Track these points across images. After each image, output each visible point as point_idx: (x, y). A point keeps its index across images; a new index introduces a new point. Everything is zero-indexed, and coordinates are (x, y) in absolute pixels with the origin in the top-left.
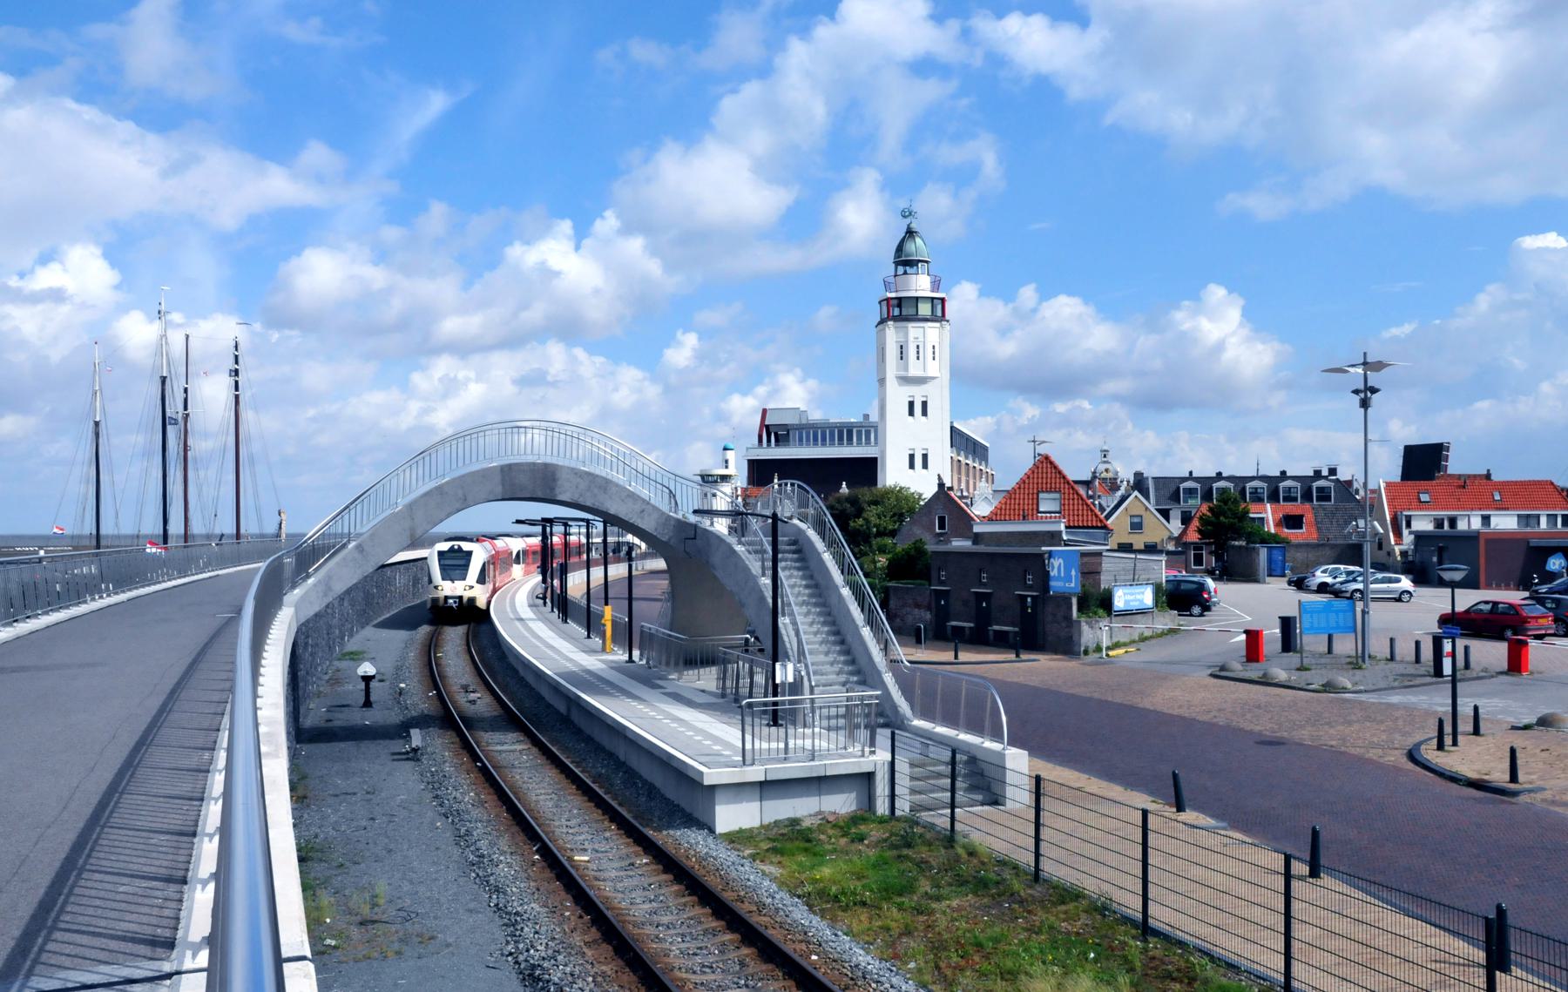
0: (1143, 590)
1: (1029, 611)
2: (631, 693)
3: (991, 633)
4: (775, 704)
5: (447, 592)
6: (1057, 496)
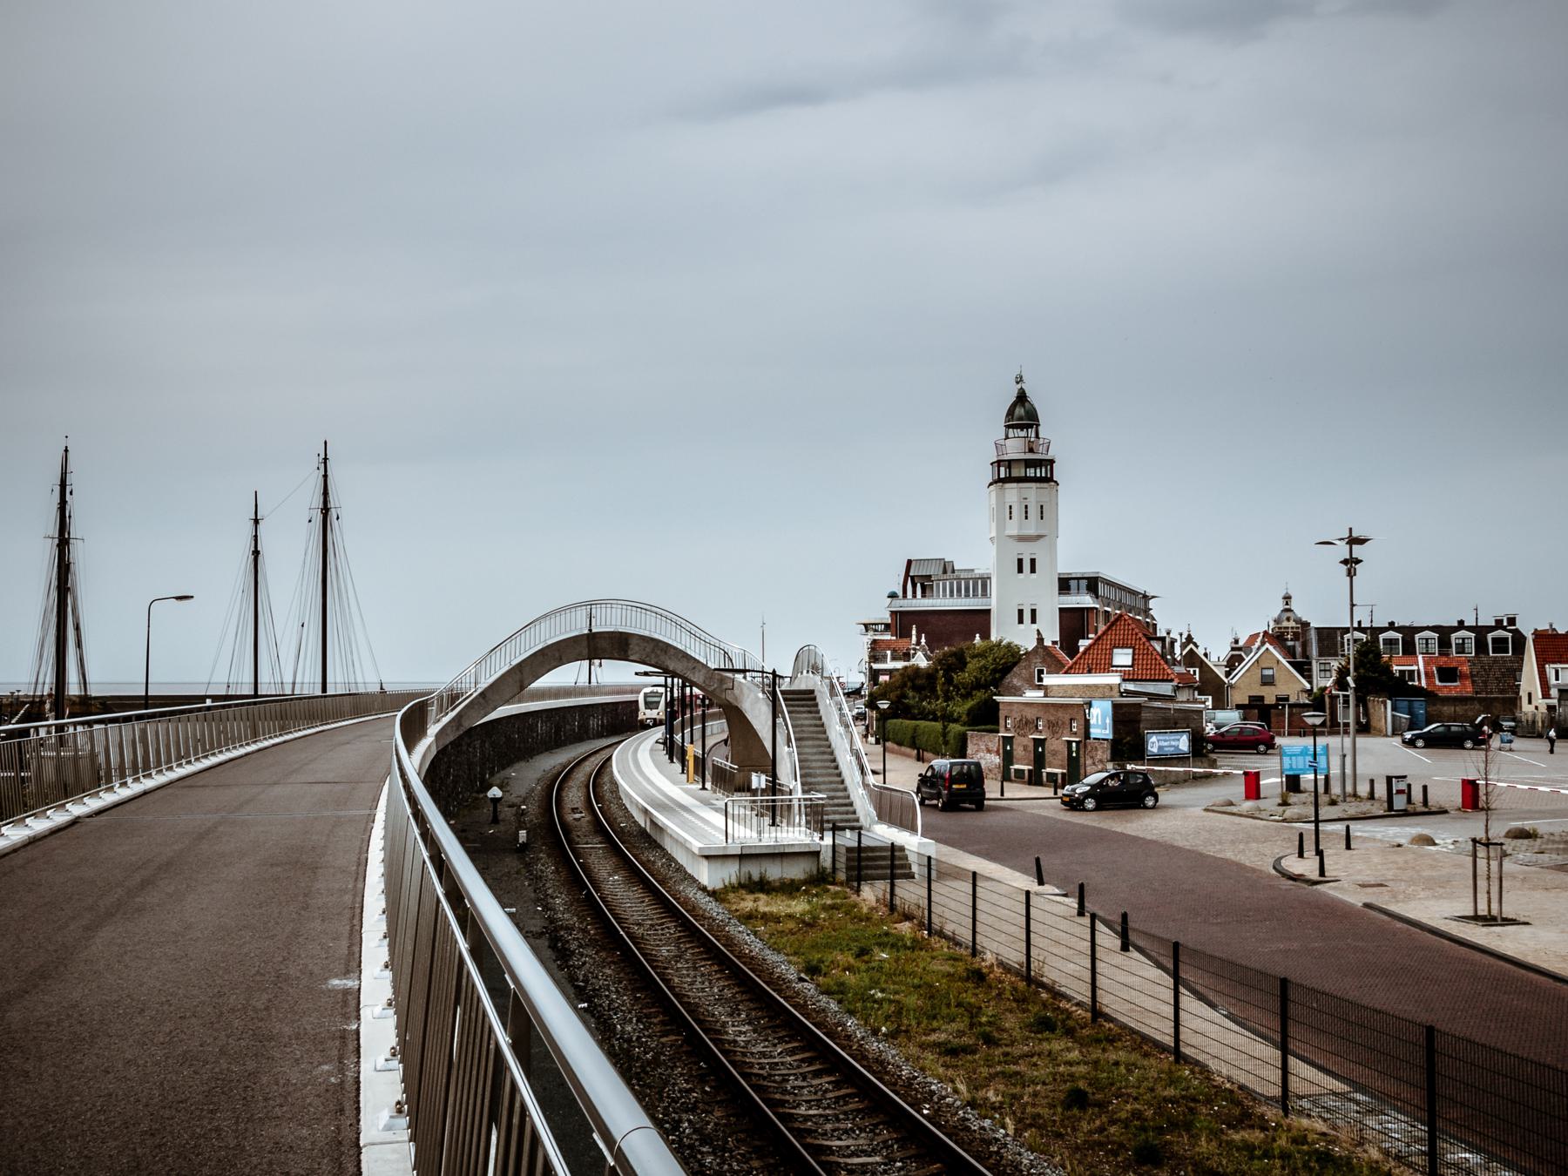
3: (1013, 770)
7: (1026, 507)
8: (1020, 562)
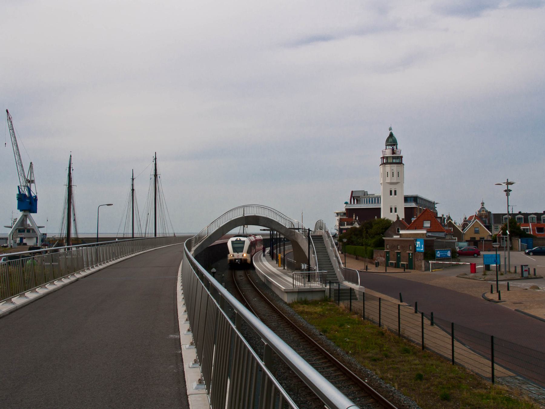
0: (446, 252)
1: (411, 257)
2: (280, 271)
4: (309, 273)
5: (236, 257)
6: (430, 222)
7: (393, 173)
8: (391, 191)
